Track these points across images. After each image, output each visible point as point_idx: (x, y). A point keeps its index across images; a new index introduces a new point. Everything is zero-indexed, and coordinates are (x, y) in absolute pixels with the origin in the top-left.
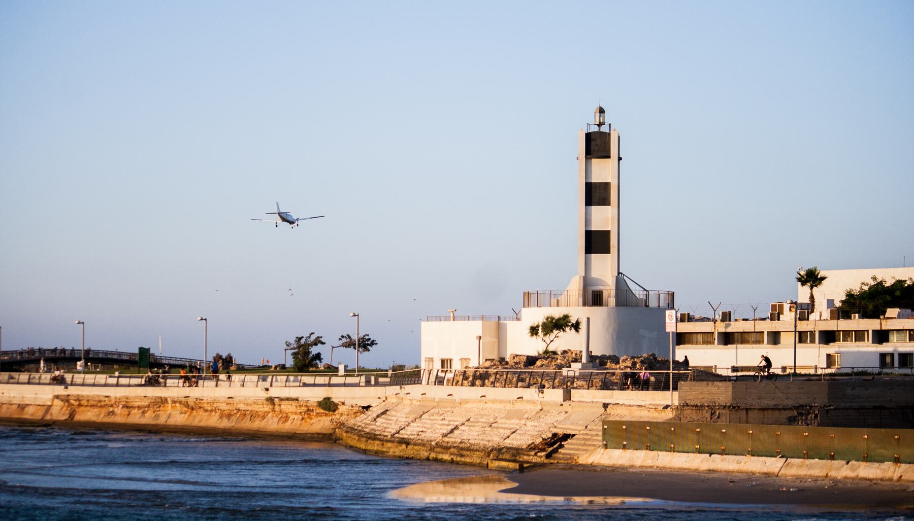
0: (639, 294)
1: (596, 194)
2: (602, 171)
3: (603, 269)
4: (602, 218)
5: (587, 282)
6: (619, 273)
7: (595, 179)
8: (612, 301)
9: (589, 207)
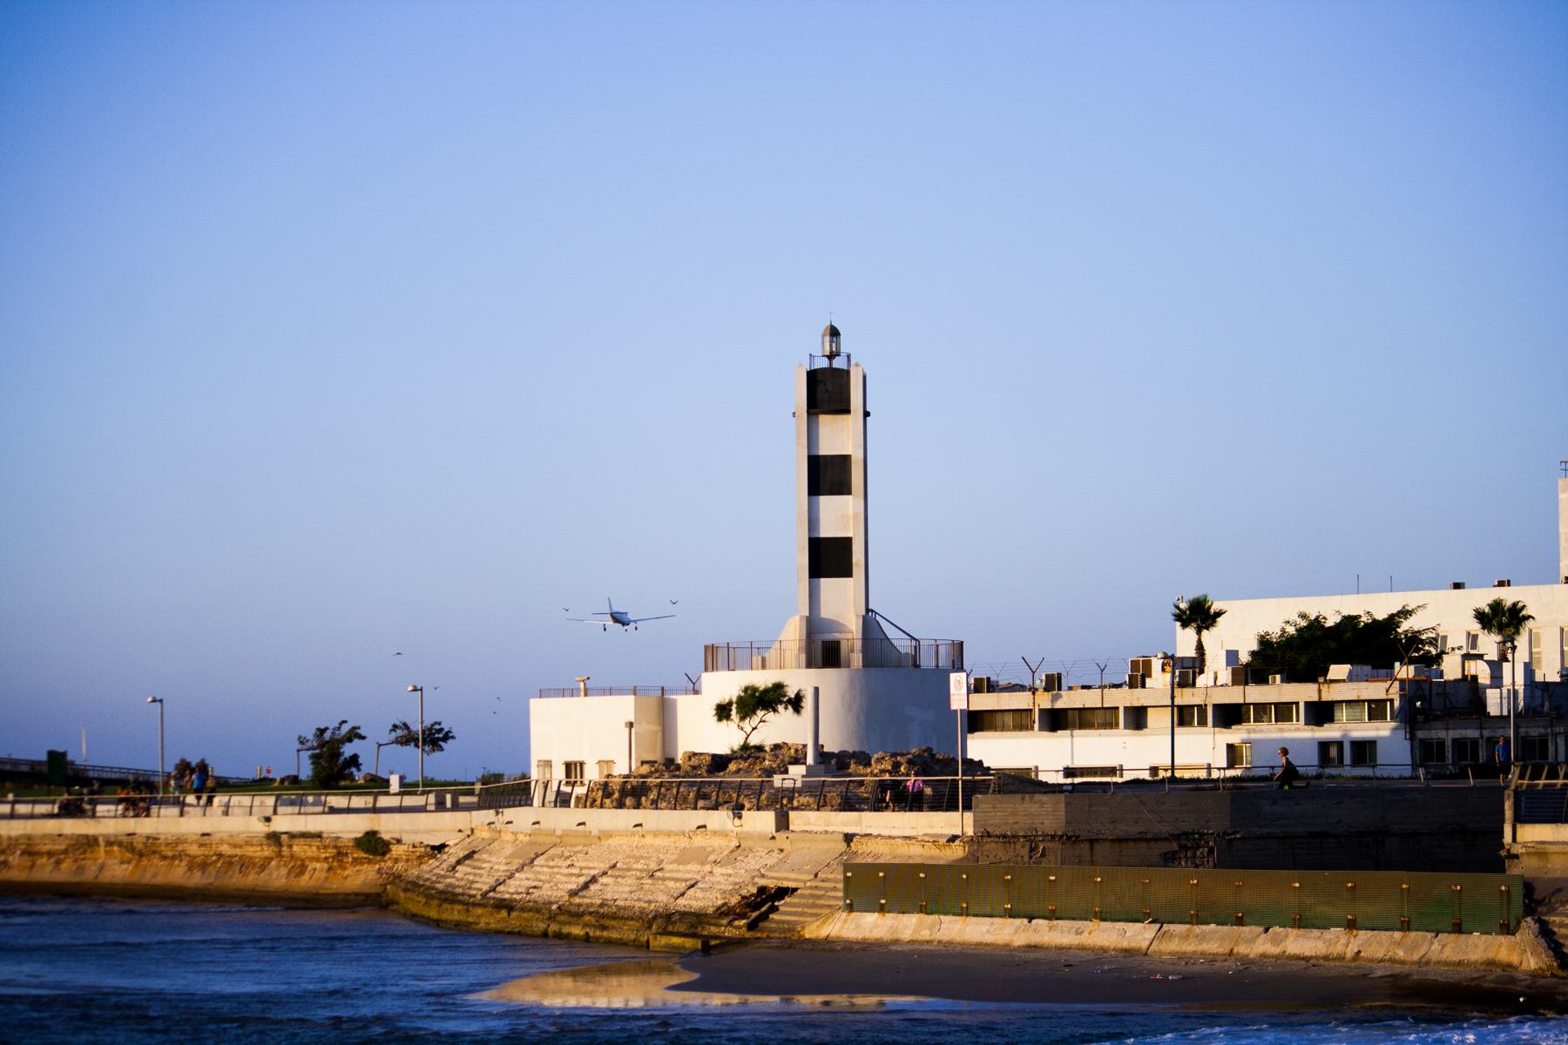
0: (903, 645)
1: (827, 475)
2: (837, 436)
3: (841, 601)
4: (838, 516)
5: (813, 625)
6: (868, 610)
7: (825, 449)
8: (857, 659)
9: (825, 583)
